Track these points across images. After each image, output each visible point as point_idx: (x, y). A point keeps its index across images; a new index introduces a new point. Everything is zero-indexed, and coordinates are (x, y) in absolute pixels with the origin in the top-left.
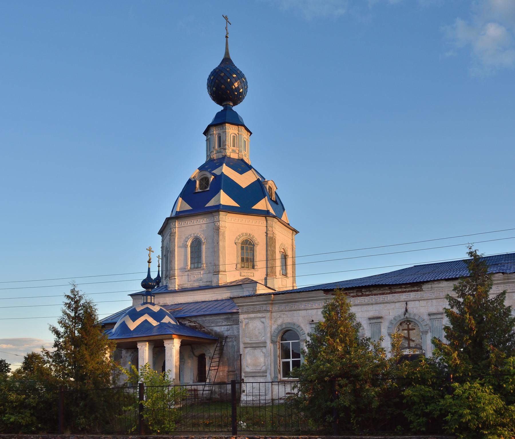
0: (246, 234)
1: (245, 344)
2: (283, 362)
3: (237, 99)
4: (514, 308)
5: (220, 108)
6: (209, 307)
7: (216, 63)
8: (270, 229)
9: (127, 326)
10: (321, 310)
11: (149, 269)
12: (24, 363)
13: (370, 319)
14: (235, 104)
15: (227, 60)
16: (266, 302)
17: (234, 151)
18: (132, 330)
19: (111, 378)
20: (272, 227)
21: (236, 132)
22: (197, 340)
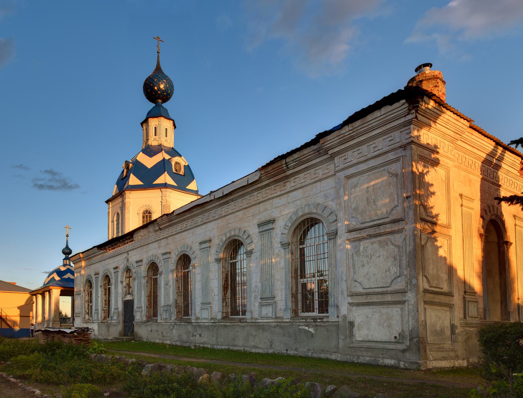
0: (146, 205)
1: (450, 306)
3: (166, 96)
5: (154, 105)
6: (352, 131)
7: (150, 71)
8: (164, 198)
10: (435, 168)
11: (67, 241)
13: (201, 243)
14: (164, 101)
15: (158, 69)
16: (384, 128)
17: (155, 139)
19: (311, 330)
22: (366, 128)
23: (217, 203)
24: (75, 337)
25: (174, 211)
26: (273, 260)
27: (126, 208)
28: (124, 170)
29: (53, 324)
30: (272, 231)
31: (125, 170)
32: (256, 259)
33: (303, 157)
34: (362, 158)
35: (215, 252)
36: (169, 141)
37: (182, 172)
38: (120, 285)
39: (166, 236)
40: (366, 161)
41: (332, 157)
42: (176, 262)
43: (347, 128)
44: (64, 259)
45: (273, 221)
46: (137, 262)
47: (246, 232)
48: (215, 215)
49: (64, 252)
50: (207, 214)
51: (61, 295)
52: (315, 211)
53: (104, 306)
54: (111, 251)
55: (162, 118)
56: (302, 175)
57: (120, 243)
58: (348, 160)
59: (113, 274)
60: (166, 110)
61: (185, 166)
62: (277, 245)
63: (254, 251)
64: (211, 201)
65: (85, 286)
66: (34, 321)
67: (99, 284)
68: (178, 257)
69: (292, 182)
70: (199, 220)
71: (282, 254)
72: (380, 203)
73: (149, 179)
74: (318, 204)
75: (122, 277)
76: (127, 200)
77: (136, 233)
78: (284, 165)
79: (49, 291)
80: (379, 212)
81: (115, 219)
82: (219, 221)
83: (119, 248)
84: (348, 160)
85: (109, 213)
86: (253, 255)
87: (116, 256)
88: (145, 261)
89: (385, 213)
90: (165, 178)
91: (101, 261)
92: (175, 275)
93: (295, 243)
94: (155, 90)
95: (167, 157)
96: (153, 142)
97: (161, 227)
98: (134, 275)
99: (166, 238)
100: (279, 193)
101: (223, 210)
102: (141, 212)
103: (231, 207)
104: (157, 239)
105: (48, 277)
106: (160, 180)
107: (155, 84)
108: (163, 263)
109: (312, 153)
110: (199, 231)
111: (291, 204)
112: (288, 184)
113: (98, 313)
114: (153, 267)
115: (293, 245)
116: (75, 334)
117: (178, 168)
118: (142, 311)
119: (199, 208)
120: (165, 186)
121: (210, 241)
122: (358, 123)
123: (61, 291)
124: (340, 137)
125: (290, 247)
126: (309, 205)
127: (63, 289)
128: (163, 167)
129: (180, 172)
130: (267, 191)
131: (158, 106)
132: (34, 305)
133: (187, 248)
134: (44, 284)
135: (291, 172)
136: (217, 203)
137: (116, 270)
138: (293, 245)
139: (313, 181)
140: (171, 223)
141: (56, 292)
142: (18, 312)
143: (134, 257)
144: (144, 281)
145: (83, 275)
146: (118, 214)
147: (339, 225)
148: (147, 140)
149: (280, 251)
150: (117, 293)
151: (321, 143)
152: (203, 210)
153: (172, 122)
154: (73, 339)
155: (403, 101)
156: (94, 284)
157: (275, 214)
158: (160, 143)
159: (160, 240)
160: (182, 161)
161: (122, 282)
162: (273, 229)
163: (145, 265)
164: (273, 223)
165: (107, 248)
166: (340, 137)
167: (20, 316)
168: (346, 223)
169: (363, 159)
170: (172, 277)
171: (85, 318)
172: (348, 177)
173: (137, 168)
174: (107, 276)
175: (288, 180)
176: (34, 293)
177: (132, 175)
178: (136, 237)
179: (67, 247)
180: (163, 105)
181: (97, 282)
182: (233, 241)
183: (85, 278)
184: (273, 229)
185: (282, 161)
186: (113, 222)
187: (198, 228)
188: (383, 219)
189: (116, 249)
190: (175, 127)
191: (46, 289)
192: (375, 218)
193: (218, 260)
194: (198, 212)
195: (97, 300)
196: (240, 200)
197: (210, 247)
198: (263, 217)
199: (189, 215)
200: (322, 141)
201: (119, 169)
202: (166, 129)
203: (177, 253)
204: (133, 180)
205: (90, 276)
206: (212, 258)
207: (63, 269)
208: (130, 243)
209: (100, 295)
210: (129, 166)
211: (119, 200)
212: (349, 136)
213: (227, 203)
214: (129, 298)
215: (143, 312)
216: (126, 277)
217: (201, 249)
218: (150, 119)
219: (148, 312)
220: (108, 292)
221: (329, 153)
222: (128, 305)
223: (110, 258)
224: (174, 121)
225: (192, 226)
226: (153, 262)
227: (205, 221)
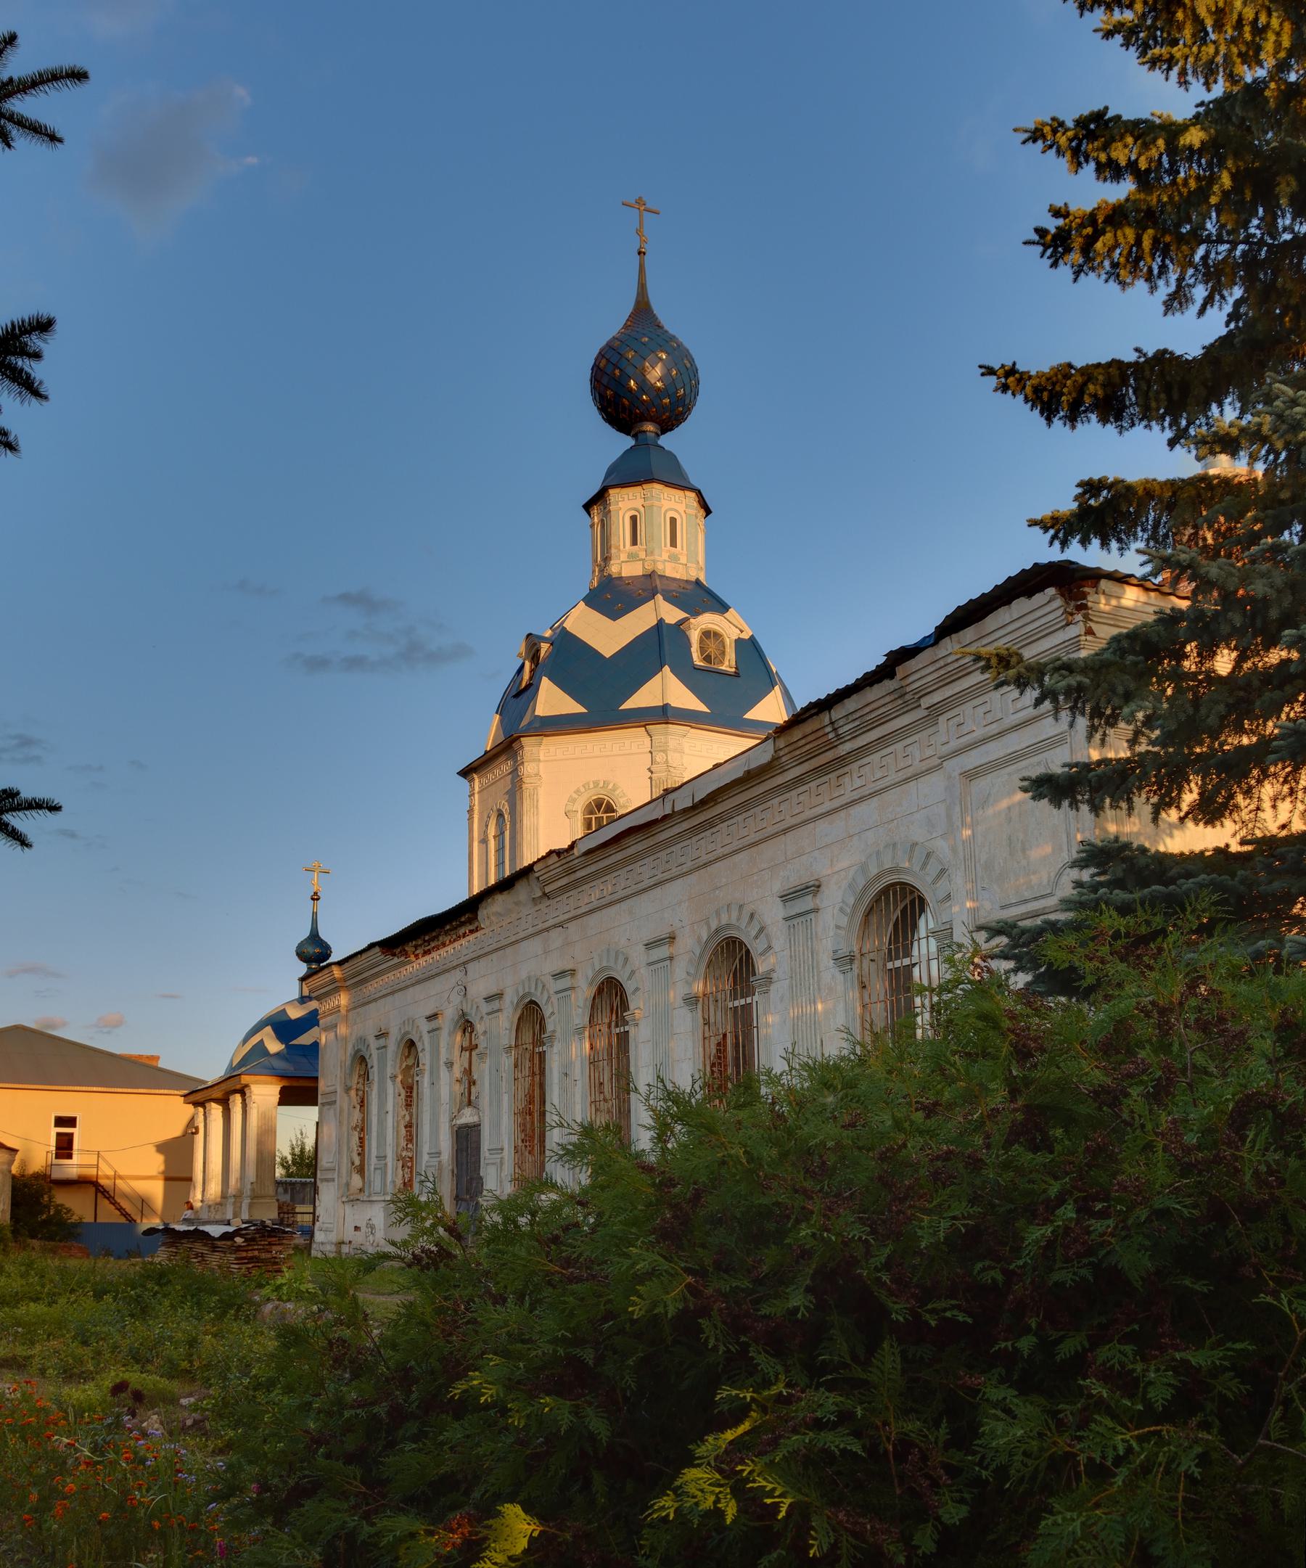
0: (596, 784)
2: (58, 1134)
3: (672, 412)
4: (1072, 498)
5: (628, 442)
7: (609, 322)
8: (659, 757)
9: (14, 1216)
11: (315, 915)
12: (1182, 854)
13: (649, 945)
14: (668, 423)
17: (632, 557)
18: (607, 653)
20: (665, 751)
21: (556, 1131)
22: (942, 672)
23: (686, 825)
24: (239, 1249)
25: (574, 843)
26: (820, 1007)
27: (526, 794)
28: (523, 666)
29: (251, 1206)
30: (812, 916)
31: (527, 664)
32: (782, 999)
33: (867, 709)
34: (994, 726)
35: (684, 975)
36: (683, 560)
37: (728, 664)
38: (444, 1072)
39: (562, 918)
40: (1001, 734)
41: (935, 712)
42: (589, 1004)
43: (949, 646)
44: (302, 979)
45: (813, 888)
46: (489, 999)
47: (756, 916)
48: (683, 860)
49: (302, 955)
50: (663, 855)
51: (281, 1103)
52: (907, 865)
53: (403, 1143)
54: (422, 961)
55: (657, 486)
56: (875, 758)
57: (446, 933)
58: (965, 729)
59: (426, 1038)
60: (672, 457)
61: (739, 642)
62: (826, 961)
63: (774, 976)
64: (665, 817)
65: (351, 1075)
66: (199, 1196)
67: (389, 1071)
68: (594, 989)
69: (855, 776)
70: (645, 871)
71: (840, 988)
72: (1035, 854)
73: (604, 690)
74: (914, 845)
75: (450, 1047)
76: (528, 769)
77: (484, 904)
78: (829, 729)
79: (242, 1091)
80: (1034, 879)
81: (492, 831)
82: (693, 878)
83: (442, 952)
84: (965, 729)
85: (471, 811)
86: (773, 987)
87: (433, 977)
88: (510, 999)
89: (1045, 882)
90: (664, 688)
91: (392, 993)
92: (587, 1046)
93: (872, 956)
94: (630, 390)
95: (672, 615)
96: (625, 566)
97: (547, 890)
98: (482, 1042)
99: (560, 925)
100: (828, 806)
101: (703, 846)
102: (580, 806)
103: (724, 837)
104: (541, 926)
105: (245, 1041)
106: (645, 697)
107: (630, 370)
108: (555, 1002)
109: (888, 699)
110: (645, 904)
111: (856, 838)
112: (846, 779)
113: (383, 1170)
114: (531, 1014)
115: (866, 963)
116: (239, 1240)
117: (712, 648)
118: (502, 1163)
119: (640, 836)
120: (664, 715)
121: (672, 938)
122: (968, 634)
123: (281, 1092)
124: (937, 665)
125: (855, 966)
126: (895, 845)
127: (285, 1083)
128: (659, 648)
129: (722, 663)
130: (801, 798)
131: (643, 444)
132: (199, 1138)
133: (617, 958)
134: (231, 1068)
135: (848, 747)
136: (686, 825)
137: (434, 1024)
138: (866, 963)
139: (902, 775)
140: (573, 877)
141: (265, 1093)
142: (157, 1163)
143: (482, 981)
144: (507, 1062)
145: (345, 1039)
146: (500, 815)
147: (956, 909)
148: (606, 559)
149: (833, 976)
150: (436, 1099)
151: (899, 676)
152: (651, 842)
153: (693, 495)
154: (232, 1257)
155: (1051, 591)
156: (375, 1069)
157: (821, 868)
158: (650, 568)
159: (547, 930)
160: (731, 627)
161: (450, 1065)
162: (816, 910)
163: (511, 1010)
164: (815, 893)
165: (409, 948)
166: (937, 665)
167: (167, 1179)
168: (968, 904)
169: (994, 729)
170: (579, 1049)
171: (348, 1185)
172: (971, 775)
173: (563, 657)
174: (411, 1044)
175: (846, 769)
176: (199, 1096)
177: (545, 680)
178: (487, 912)
179: (314, 937)
180: (665, 441)
181: (382, 1060)
182: (728, 944)
183: (350, 1050)
184: (816, 910)
185: (821, 716)
186: (484, 841)
187: (644, 896)
188: (1036, 899)
189: (434, 954)
190: (708, 512)
191: (231, 1085)
192: (1027, 895)
193: (691, 1001)
194: (640, 847)
195: (381, 1123)
196: (740, 818)
197: (671, 958)
198: (793, 876)
199: (619, 856)
200: (900, 671)
201: (506, 661)
202: (673, 521)
203: (590, 974)
204: (551, 700)
205: (362, 1040)
206: (676, 995)
207: (295, 1013)
208: (471, 937)
209: (390, 1107)
210: (538, 651)
211: (504, 767)
212: (956, 665)
213: (709, 824)
214: (468, 1117)
215: (506, 1167)
216: (463, 1049)
217: (650, 964)
218: (611, 491)
219: (519, 1165)
220: (410, 1093)
221: (923, 706)
222: (467, 1140)
223: (418, 982)
224: (699, 493)
225: (629, 891)
226: (532, 1002)
227: (661, 877)
